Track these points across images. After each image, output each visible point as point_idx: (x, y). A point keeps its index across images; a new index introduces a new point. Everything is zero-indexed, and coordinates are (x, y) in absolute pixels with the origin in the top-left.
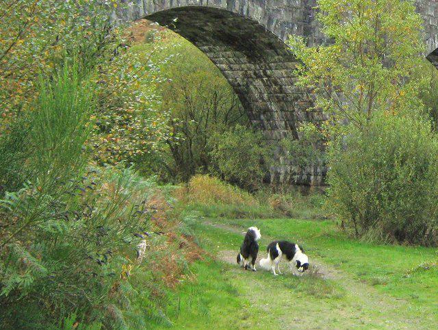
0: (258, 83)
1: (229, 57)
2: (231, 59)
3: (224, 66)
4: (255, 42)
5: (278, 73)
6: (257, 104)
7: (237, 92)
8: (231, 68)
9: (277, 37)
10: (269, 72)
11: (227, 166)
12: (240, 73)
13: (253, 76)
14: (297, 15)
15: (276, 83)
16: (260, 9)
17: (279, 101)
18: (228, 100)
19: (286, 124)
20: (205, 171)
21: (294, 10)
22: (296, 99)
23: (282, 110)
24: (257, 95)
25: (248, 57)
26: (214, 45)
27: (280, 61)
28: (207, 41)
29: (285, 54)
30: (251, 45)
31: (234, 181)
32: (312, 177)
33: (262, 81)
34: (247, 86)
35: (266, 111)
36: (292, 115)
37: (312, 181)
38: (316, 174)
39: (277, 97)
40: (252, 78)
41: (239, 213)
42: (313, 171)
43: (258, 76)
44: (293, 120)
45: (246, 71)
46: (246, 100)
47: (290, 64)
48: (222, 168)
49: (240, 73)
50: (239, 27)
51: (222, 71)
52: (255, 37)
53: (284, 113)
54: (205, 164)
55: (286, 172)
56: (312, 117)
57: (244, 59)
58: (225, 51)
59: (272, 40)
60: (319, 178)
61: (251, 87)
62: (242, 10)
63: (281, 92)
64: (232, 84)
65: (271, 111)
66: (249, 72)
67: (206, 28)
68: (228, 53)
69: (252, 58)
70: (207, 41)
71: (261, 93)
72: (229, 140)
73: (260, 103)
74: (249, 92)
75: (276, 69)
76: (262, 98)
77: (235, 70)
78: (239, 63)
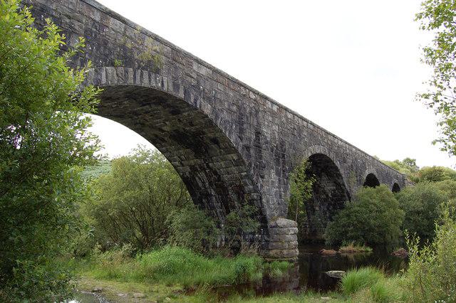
2: (183, 157)
3: (177, 163)
9: (221, 131)
10: (211, 164)
14: (234, 117)
24: (200, 184)
35: (208, 195)
43: (203, 169)
50: (191, 124)
52: (204, 133)
55: (222, 240)
62: (196, 103)
64: (182, 177)
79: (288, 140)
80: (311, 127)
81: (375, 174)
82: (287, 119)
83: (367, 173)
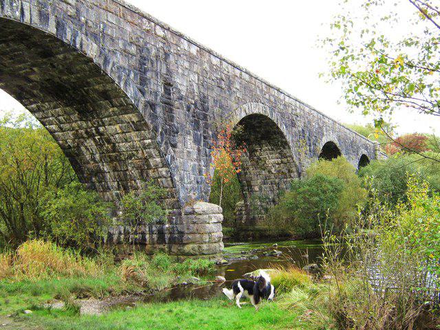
0: (90, 143)
1: (59, 115)
3: (54, 127)
4: (87, 92)
5: (111, 129)
6: (89, 166)
7: (67, 155)
8: (61, 129)
10: (101, 129)
11: (63, 228)
12: (70, 133)
13: (85, 135)
15: (109, 141)
16: (95, 45)
17: (112, 161)
18: (58, 163)
19: (118, 185)
20: (38, 236)
21: (130, 56)
22: (130, 157)
23: (115, 170)
24: (88, 157)
25: (80, 113)
26: (43, 102)
27: (115, 114)
28: (34, 96)
29: (121, 105)
30: (83, 96)
31: (70, 244)
32: (147, 236)
33: (95, 140)
34: (78, 147)
35: (99, 173)
36: (125, 175)
37: (148, 240)
38: (151, 232)
39: (110, 157)
40: (83, 138)
41: (82, 290)
42: (147, 230)
43: (91, 136)
44: (126, 180)
45: (77, 131)
46: (77, 163)
47: (126, 116)
48: (56, 231)
49: (70, 133)
51: (52, 132)
53: (116, 173)
54: (40, 228)
55: (120, 233)
56: (147, 175)
57: (75, 116)
58: (55, 108)
59: (108, 87)
60: (155, 236)
61: (83, 148)
62: (74, 41)
63: (114, 151)
65: (103, 172)
66: (79, 131)
67: (32, 77)
68: (57, 110)
69: (84, 114)
70: (34, 96)
71: (92, 154)
72: (65, 201)
73: (91, 165)
74: (80, 153)
75: (110, 125)
76: (94, 159)
77: (65, 131)
78: (69, 121)
79: (212, 95)
80: (246, 77)
81: (336, 141)
82: (211, 65)
83: (325, 140)
